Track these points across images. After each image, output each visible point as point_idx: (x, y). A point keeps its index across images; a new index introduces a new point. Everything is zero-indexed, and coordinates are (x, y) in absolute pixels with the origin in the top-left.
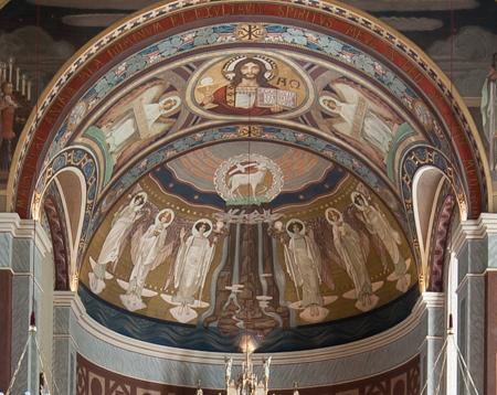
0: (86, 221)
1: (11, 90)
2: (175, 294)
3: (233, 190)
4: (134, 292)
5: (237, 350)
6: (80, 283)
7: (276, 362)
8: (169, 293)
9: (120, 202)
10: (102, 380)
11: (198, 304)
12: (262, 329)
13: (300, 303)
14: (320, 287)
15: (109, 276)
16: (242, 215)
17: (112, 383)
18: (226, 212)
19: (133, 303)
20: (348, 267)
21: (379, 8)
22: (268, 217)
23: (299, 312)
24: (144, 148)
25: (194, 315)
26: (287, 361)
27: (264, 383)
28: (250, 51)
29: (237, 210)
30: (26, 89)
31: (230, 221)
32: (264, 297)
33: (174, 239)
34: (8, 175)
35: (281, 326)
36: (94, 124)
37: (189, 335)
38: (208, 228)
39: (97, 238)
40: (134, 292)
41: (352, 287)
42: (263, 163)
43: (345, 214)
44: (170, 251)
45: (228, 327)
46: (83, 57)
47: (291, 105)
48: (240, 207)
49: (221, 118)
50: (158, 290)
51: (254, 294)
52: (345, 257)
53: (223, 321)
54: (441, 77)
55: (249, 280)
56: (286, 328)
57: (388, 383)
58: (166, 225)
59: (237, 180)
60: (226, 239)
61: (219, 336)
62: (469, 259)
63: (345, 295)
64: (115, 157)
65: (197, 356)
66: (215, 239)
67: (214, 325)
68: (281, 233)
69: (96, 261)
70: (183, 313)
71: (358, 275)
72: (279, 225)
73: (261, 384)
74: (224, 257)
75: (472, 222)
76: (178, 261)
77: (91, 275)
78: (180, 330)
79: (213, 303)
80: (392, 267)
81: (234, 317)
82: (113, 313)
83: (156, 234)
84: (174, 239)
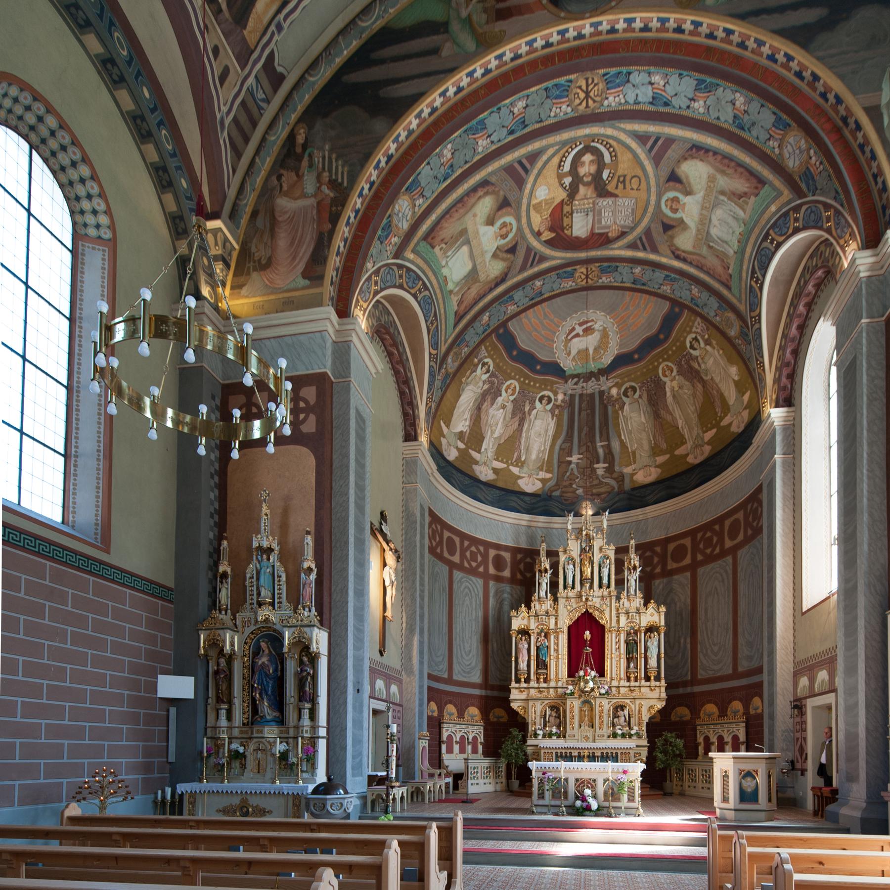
0: (432, 375)
1: (327, 179)
2: (521, 467)
3: (571, 357)
4: (485, 463)
5: (578, 514)
6: (431, 443)
7: (611, 523)
8: (517, 466)
9: (466, 364)
10: (457, 540)
11: (543, 475)
12: (599, 495)
13: (633, 467)
14: (652, 448)
15: (461, 446)
16: (581, 384)
17: (481, 569)
18: (566, 382)
19: (485, 473)
20: (680, 423)
21: (746, 7)
22: (605, 384)
23: (633, 475)
24: (484, 295)
25: (539, 485)
26: (623, 521)
27: (603, 534)
28: (586, 131)
29: (576, 380)
30: (341, 172)
31: (570, 392)
32: (601, 465)
33: (520, 413)
34: (325, 270)
35: (616, 489)
36: (425, 238)
37: (534, 503)
38: (549, 401)
39: (445, 401)
40: (485, 463)
41: (683, 442)
42: (600, 320)
43: (679, 366)
44: (517, 424)
45: (568, 495)
46: (401, 132)
47: (629, 222)
48: (578, 376)
49: (559, 256)
50: (507, 462)
51: (592, 463)
52: (677, 413)
54: (828, 78)
55: (588, 450)
56: (621, 491)
57: (694, 558)
58: (512, 398)
59: (577, 344)
60: (566, 411)
61: (562, 503)
62: (864, 303)
63: (677, 452)
64: (455, 299)
65: (541, 521)
66: (557, 412)
67: (557, 493)
68: (617, 400)
69: (448, 426)
70: (530, 484)
71: (691, 429)
72: (614, 391)
73: (600, 536)
74: (565, 428)
75: (868, 253)
76: (524, 435)
77: (444, 441)
78: (527, 499)
80: (726, 408)
81: (574, 486)
82: (467, 481)
83: (504, 407)
84: (520, 413)
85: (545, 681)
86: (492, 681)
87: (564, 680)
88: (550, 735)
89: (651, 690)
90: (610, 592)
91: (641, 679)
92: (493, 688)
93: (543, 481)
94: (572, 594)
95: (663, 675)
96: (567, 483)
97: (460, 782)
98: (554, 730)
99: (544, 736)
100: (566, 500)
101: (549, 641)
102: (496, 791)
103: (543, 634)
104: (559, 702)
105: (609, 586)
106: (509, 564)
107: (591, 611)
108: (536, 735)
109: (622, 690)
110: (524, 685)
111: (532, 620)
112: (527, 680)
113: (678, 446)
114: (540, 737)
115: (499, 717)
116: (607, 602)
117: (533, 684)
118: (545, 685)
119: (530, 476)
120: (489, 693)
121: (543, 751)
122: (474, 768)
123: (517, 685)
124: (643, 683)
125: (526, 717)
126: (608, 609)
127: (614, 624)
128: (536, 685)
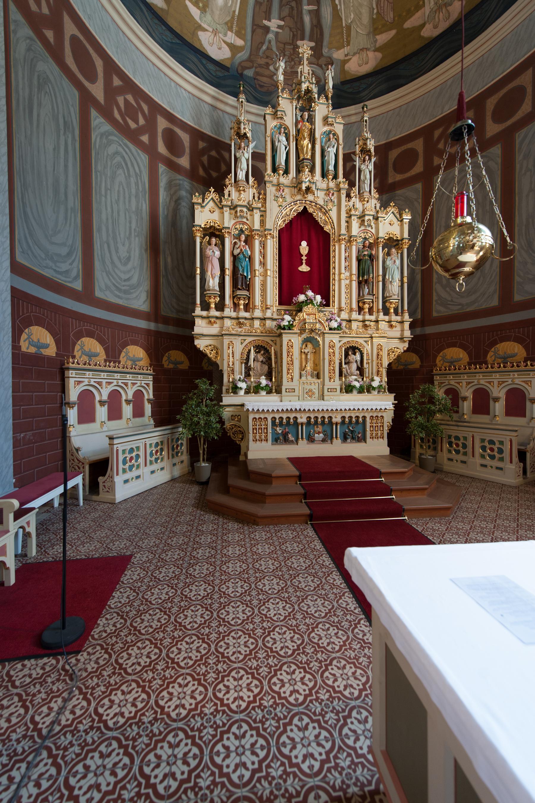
11: (231, 37)
13: (346, 50)
14: (373, 21)
23: (345, 62)
45: (264, 79)
53: (258, 70)
55: (291, 15)
61: (255, 88)
63: (407, 25)
78: (211, 67)
79: (249, 43)
85: (247, 308)
86: (165, 311)
87: (275, 309)
88: (256, 389)
89: (391, 326)
90: (338, 185)
91: (378, 311)
92: (166, 321)
93: (231, 46)
94: (285, 180)
95: (406, 308)
96: (262, 61)
97: (101, 479)
98: (264, 382)
99: (247, 392)
100: (261, 86)
101: (252, 248)
102: (173, 480)
103: (243, 237)
104: (268, 339)
105: (335, 177)
106: (187, 150)
107: (310, 210)
108: (235, 389)
109: (354, 325)
110: (214, 313)
111: (227, 212)
112: (220, 307)
113: (410, 14)
114: (242, 392)
115: (176, 363)
116: (334, 198)
117: (228, 312)
118: (247, 315)
119: (215, 32)
120: (162, 328)
121: (251, 417)
122: (132, 450)
123: (204, 313)
124: (381, 316)
125: (218, 362)
126: (335, 209)
127: (343, 231)
128: (234, 315)
